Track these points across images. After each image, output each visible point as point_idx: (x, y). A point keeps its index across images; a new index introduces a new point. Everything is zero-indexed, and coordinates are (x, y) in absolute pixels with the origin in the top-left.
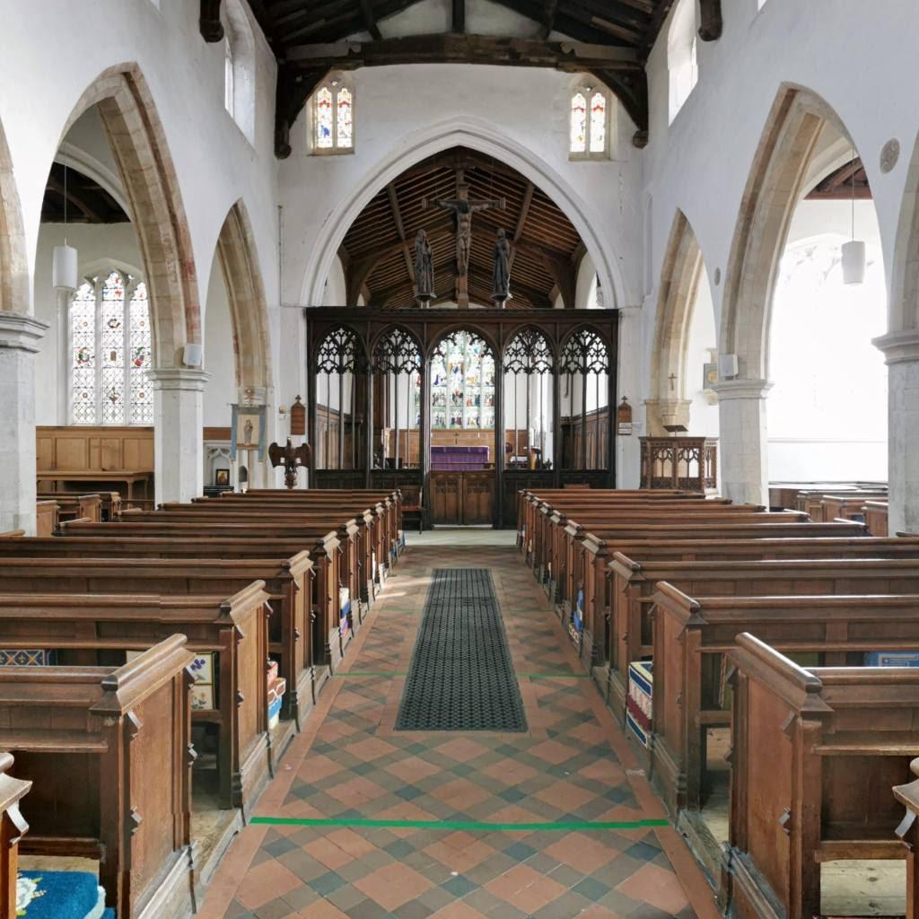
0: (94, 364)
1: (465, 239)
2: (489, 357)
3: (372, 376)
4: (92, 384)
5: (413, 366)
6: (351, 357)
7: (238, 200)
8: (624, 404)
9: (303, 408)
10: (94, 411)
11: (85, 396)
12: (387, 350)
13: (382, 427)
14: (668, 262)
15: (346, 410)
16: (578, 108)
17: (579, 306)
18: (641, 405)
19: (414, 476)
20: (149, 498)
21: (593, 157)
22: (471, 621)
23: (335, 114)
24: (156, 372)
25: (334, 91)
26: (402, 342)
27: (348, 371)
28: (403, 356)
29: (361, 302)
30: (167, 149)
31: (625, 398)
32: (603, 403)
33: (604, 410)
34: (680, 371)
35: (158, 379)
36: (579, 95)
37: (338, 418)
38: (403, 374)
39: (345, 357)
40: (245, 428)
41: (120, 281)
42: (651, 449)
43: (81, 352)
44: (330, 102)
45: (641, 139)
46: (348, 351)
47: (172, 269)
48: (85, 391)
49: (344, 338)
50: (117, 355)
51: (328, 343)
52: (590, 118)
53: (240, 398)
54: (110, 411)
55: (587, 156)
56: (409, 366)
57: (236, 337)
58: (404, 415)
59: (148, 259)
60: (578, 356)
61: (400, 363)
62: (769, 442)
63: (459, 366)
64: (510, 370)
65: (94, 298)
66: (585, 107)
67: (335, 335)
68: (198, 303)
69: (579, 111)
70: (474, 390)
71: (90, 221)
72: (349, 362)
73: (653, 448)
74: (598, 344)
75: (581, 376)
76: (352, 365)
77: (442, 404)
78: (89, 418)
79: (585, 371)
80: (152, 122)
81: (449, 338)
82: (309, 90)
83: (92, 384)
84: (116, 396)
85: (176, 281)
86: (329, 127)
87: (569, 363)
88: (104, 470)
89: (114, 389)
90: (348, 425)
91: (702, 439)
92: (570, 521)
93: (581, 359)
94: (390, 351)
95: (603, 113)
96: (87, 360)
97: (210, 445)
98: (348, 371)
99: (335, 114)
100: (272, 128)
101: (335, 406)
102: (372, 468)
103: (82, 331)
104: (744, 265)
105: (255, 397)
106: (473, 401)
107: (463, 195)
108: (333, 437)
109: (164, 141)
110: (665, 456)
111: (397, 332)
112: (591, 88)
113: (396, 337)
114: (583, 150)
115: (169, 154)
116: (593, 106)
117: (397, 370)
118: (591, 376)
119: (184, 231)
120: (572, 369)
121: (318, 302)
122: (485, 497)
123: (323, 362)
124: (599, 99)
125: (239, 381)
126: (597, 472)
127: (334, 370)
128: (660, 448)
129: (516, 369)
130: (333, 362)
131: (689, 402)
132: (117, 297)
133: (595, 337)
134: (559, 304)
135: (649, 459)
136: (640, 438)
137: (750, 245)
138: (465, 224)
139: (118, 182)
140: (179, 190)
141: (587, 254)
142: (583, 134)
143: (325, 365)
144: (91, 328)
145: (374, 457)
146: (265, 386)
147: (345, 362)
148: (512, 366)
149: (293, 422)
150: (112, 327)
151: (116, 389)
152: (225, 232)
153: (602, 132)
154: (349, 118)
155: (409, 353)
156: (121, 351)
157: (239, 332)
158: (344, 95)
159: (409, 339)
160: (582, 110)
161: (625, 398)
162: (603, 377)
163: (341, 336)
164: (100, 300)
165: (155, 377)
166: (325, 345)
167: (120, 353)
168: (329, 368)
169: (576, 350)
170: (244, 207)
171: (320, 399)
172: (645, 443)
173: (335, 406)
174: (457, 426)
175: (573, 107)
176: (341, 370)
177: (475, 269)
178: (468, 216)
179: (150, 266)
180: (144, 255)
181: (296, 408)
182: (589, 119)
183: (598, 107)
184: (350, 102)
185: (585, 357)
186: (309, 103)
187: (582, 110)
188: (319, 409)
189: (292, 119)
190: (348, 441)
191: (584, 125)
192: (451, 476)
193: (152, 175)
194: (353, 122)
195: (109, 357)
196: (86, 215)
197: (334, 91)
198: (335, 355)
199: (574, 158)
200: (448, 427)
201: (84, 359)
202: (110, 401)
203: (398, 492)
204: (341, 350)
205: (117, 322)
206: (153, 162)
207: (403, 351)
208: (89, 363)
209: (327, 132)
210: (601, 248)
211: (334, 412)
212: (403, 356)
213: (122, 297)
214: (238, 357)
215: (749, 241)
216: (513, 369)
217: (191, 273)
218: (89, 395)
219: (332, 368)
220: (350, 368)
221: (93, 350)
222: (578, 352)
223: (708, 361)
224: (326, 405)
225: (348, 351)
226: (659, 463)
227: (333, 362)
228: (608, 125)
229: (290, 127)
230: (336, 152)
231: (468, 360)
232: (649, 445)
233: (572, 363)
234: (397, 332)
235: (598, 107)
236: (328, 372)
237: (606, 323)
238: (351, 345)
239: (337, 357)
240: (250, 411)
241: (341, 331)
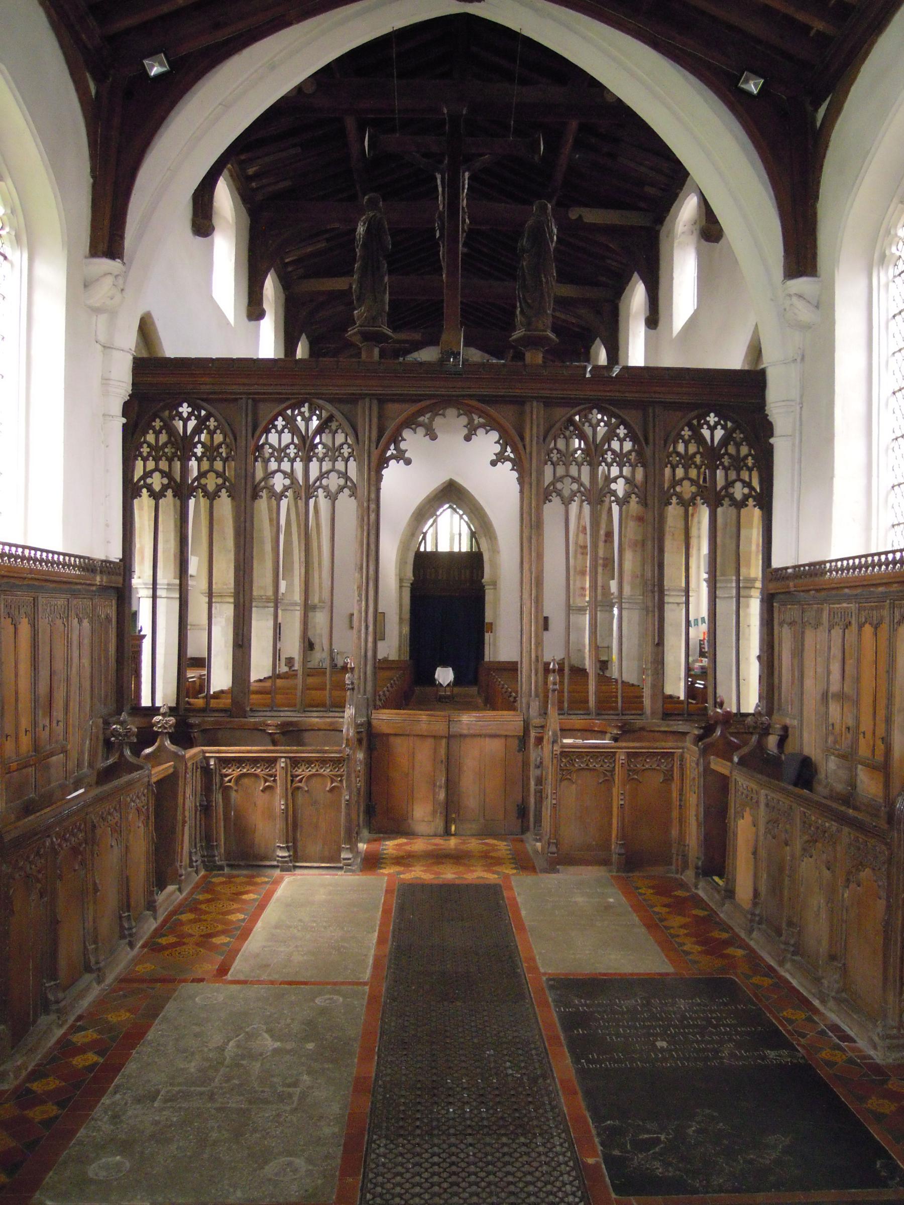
2: (508, 465)
5: (342, 482)
29: (301, 351)
39: (314, 466)
51: (157, 433)
56: (568, 487)
60: (579, 465)
74: (621, 441)
81: (420, 425)
87: (680, 482)
93: (299, 466)
123: (322, 476)
133: (207, 418)
143: (325, 482)
162: (347, 505)
166: (150, 437)
169: (746, 457)
185: (184, 460)
198: (579, 465)
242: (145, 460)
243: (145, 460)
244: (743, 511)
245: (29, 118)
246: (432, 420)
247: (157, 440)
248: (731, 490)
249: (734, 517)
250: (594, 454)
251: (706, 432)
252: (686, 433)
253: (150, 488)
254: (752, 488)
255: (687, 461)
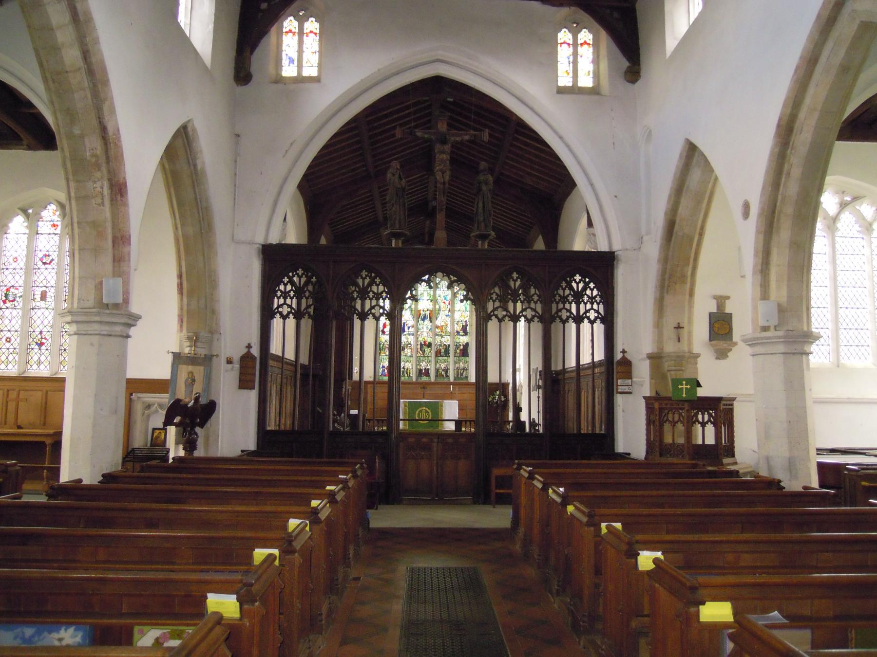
0: (21, 304)
1: (442, 172)
3: (334, 323)
4: (17, 327)
6: (310, 301)
7: (189, 121)
8: (624, 358)
9: (253, 358)
10: (17, 358)
11: (8, 340)
12: (353, 292)
13: (343, 380)
14: (673, 198)
15: (304, 359)
16: (564, 43)
17: (563, 246)
18: (643, 359)
19: (380, 440)
20: (51, 463)
21: (582, 91)
22: (435, 580)
23: (301, 43)
24: (70, 312)
25: (301, 21)
26: (370, 284)
27: (306, 316)
28: (371, 299)
30: (100, 50)
31: (624, 352)
32: (600, 356)
33: (600, 363)
34: (686, 321)
35: (73, 322)
36: (564, 30)
37: (293, 368)
38: (370, 323)
39: (304, 301)
40: (186, 381)
41: (58, 213)
42: (659, 409)
43: (8, 290)
44: (297, 31)
45: (633, 73)
46: (307, 294)
47: (99, 189)
48: (8, 335)
49: (303, 280)
50: (48, 294)
51: (285, 285)
52: (579, 55)
53: (181, 346)
54: (36, 358)
55: (574, 90)
56: (377, 311)
57: (180, 276)
58: (369, 362)
59: (71, 177)
61: (367, 307)
62: (815, 402)
63: (428, 313)
64: (493, 318)
65: (27, 231)
66: (571, 42)
67: (294, 276)
68: (129, 231)
69: (565, 46)
70: (443, 340)
71: (30, 148)
72: (308, 307)
73: (661, 410)
74: (592, 290)
75: (574, 325)
76: (311, 310)
77: (409, 354)
78: (10, 366)
79: (579, 320)
80: (82, 18)
82: (274, 16)
83: (17, 327)
84: (44, 341)
85: (103, 204)
86: (295, 56)
87: (560, 310)
88: (19, 427)
89: (41, 333)
90: (305, 376)
91: (719, 399)
92: (537, 476)
93: (574, 306)
94: (355, 295)
95: (591, 50)
96: (14, 300)
97: (146, 399)
98: (306, 316)
99: (301, 43)
100: (233, 54)
101: (290, 355)
102: (331, 429)
103: (11, 267)
104: (780, 197)
105: (199, 344)
106: (443, 351)
107: (442, 127)
108: (288, 391)
109: (96, 41)
110: (676, 419)
111: (364, 273)
112: (578, 24)
113: (364, 279)
114: (570, 84)
115: (102, 55)
116: (580, 42)
117: (363, 317)
118: (585, 325)
119: (116, 144)
120: (564, 318)
121: (274, 239)
122: (463, 466)
123: (279, 306)
124: (585, 35)
125: (181, 326)
126: (593, 437)
127: (291, 316)
128: (671, 409)
129: (500, 316)
130: (290, 306)
131: (698, 356)
132: (52, 230)
133: (589, 283)
134: (540, 245)
135: (657, 423)
136: (644, 397)
137: (788, 174)
138: (444, 156)
139: (40, 87)
140: (112, 98)
141: (576, 189)
142: (570, 69)
144: (22, 264)
145: (334, 415)
146: (211, 332)
147: (303, 306)
148: (496, 313)
149: (241, 374)
150: (45, 263)
151: (44, 333)
152: (170, 153)
153: (591, 67)
154: (316, 47)
155: (378, 296)
156: (53, 290)
157: (184, 269)
158: (312, 25)
159: (378, 280)
160: (569, 44)
161: (624, 352)
162: (599, 328)
163: (300, 277)
164: (34, 233)
165: (69, 318)
166: (282, 287)
167: (51, 293)
168: (285, 313)
169: (568, 296)
170: (194, 130)
171: (275, 348)
172: (652, 404)
173: (290, 355)
174: (424, 379)
175: (559, 41)
176: (298, 315)
177: (450, 213)
178: (447, 148)
179: (72, 184)
180: (66, 173)
181: (246, 359)
182: (575, 54)
183: (585, 43)
184: (318, 31)
186: (274, 30)
187: (569, 44)
188: (273, 360)
189: (254, 47)
190: (304, 394)
191: (571, 59)
192: (424, 440)
193: (79, 80)
194: (320, 52)
195: (38, 297)
196: (25, 142)
197: (301, 21)
199: (562, 91)
200: (414, 380)
201: (11, 298)
202: (37, 347)
203: (362, 464)
204: (299, 293)
205: (51, 258)
206: (81, 63)
207: (371, 295)
208: (15, 303)
209: (291, 61)
210: (592, 185)
211: (289, 363)
212: (371, 299)
213: (58, 231)
214: (182, 300)
215: (786, 167)
216: (496, 316)
217: (122, 196)
218: (13, 340)
219: (289, 313)
220: (309, 313)
221: (21, 289)
222: (571, 298)
223: (714, 310)
224: (280, 354)
225: (307, 294)
226: (667, 427)
227: (290, 306)
228: (596, 61)
229: (252, 52)
230: (300, 80)
231: (437, 307)
232: (656, 406)
233: (592, 311)
234: (364, 273)
235: (585, 43)
236: (284, 317)
237: (600, 267)
238: (310, 288)
239: (294, 300)
240: (192, 360)
241: (300, 272)
242: (279, 298)
243: (279, 298)
244: (503, 323)
245: (170, 180)
246: (455, 281)
247: (285, 289)
248: (560, 314)
249: (282, 325)
250: (578, 297)
251: (574, 285)
252: (564, 284)
253: (588, 318)
254: (571, 313)
255: (285, 295)
